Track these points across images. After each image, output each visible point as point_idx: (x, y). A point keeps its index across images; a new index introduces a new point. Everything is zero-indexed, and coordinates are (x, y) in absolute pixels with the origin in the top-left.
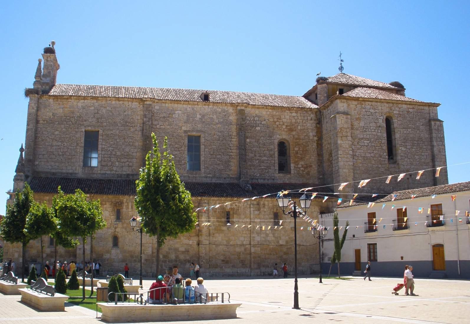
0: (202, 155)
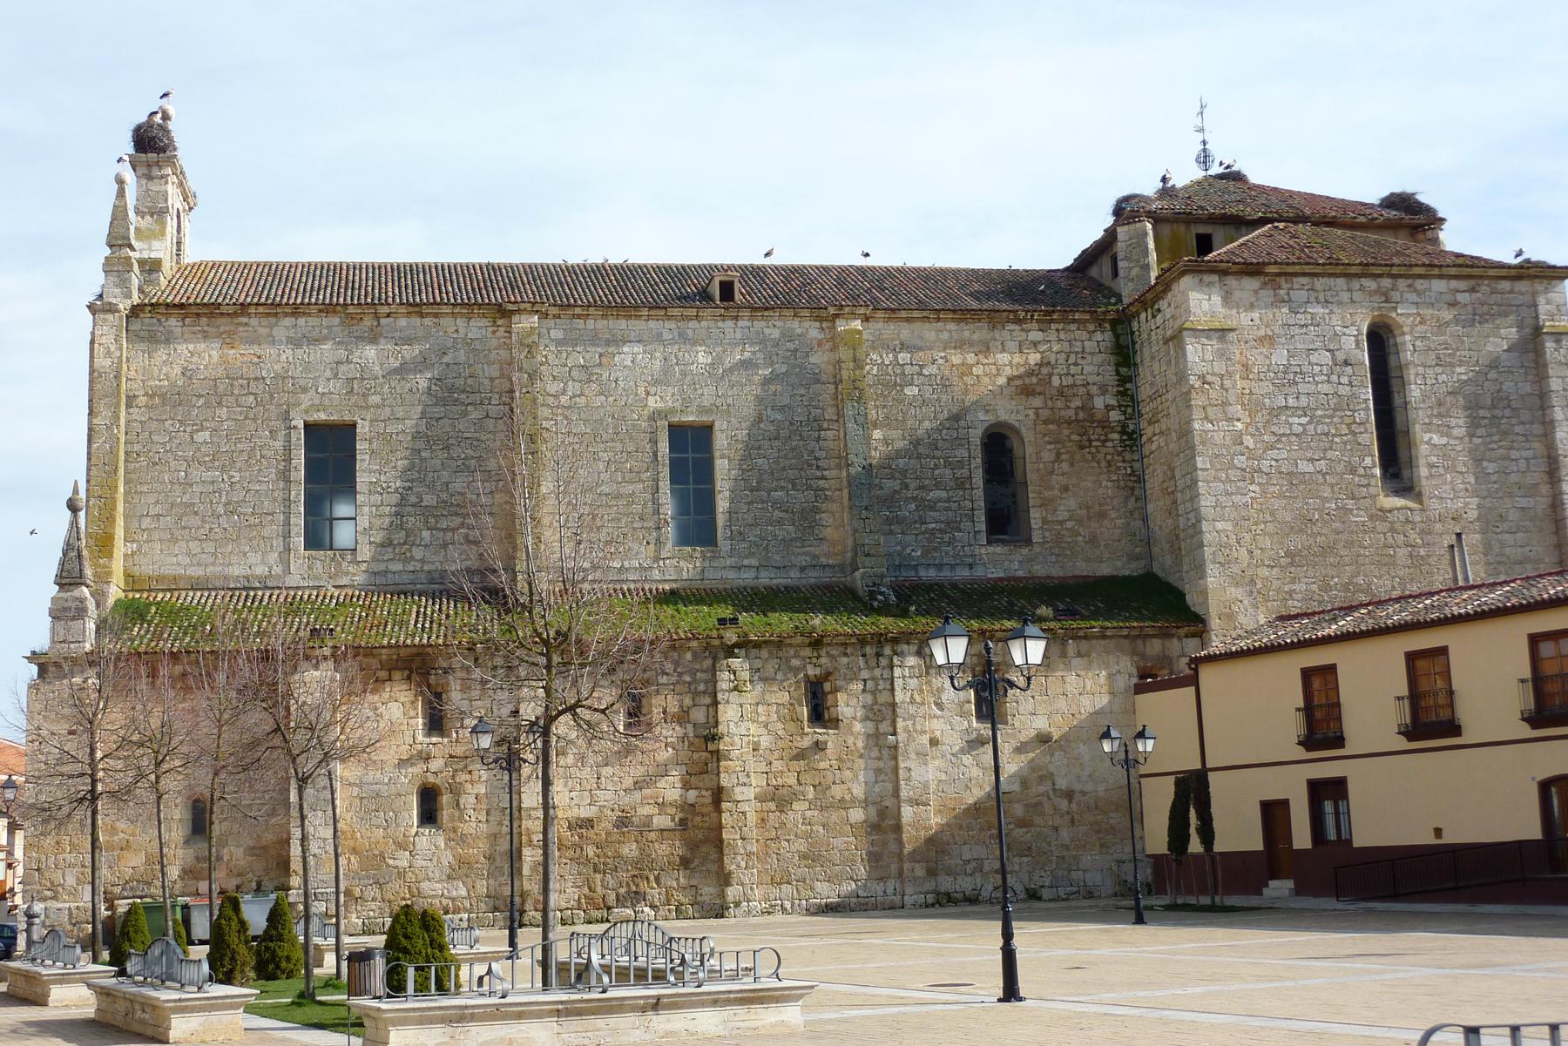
0: (720, 492)
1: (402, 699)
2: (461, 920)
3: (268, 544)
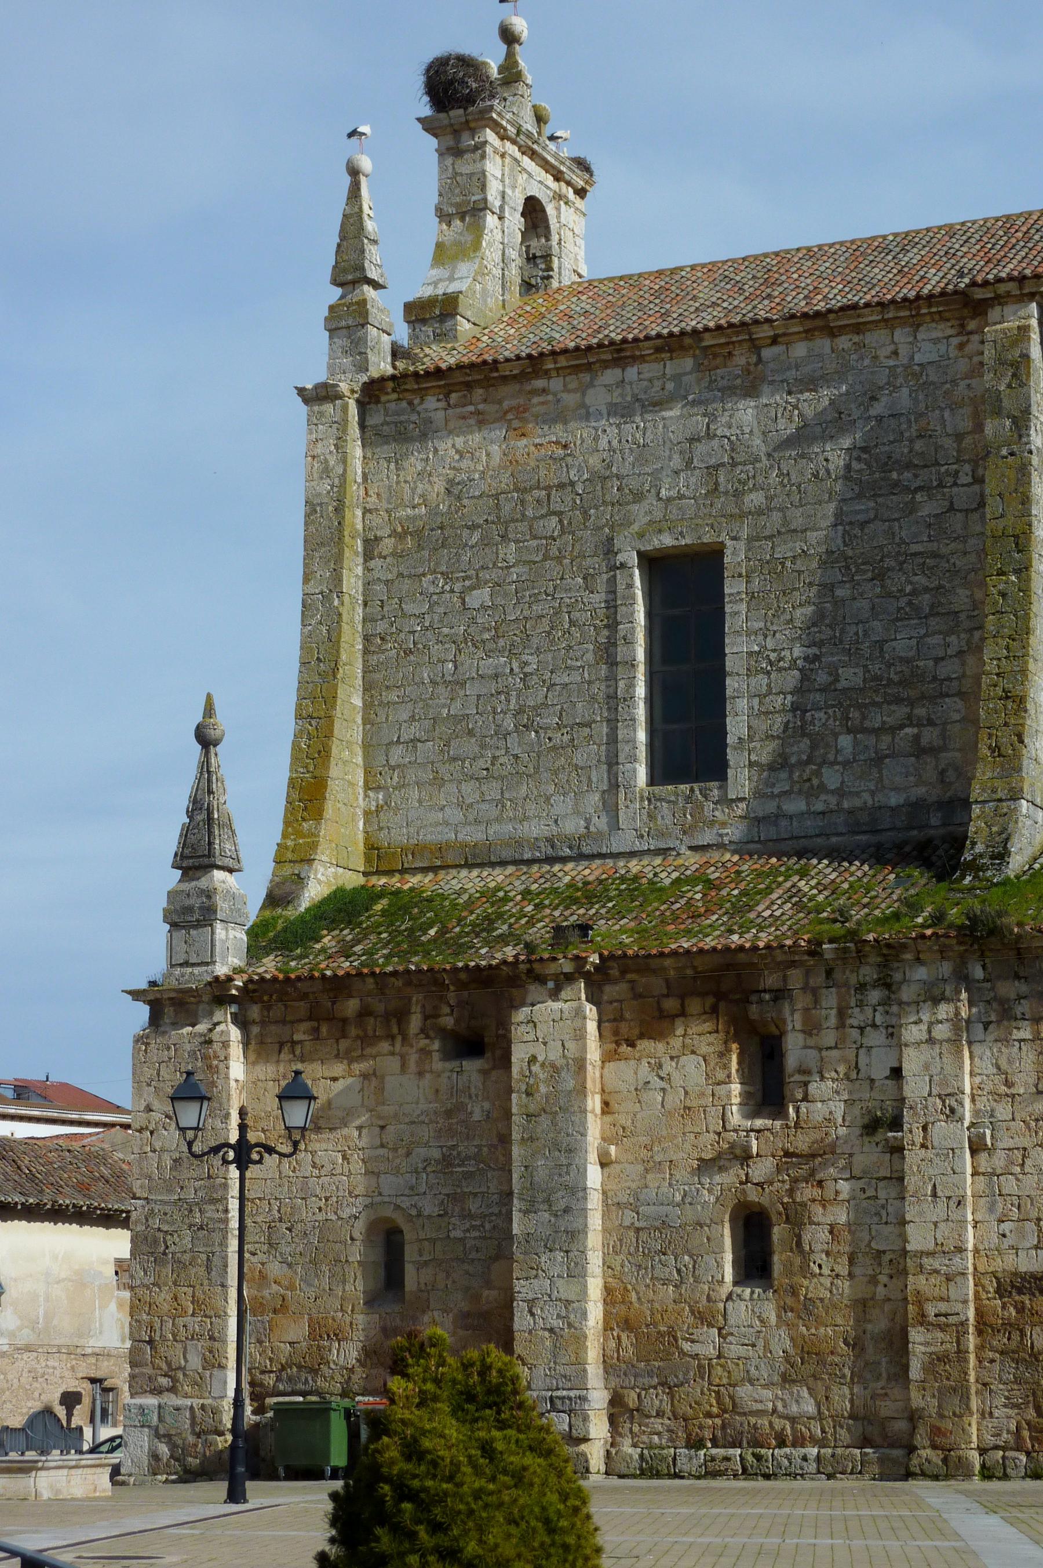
1: (704, 1049)
2: (805, 1459)
3: (584, 779)
